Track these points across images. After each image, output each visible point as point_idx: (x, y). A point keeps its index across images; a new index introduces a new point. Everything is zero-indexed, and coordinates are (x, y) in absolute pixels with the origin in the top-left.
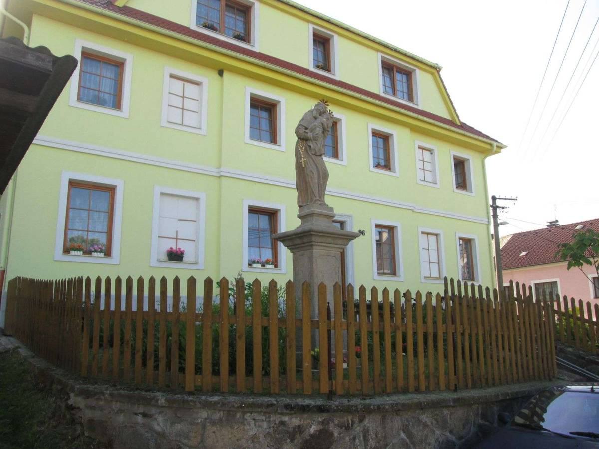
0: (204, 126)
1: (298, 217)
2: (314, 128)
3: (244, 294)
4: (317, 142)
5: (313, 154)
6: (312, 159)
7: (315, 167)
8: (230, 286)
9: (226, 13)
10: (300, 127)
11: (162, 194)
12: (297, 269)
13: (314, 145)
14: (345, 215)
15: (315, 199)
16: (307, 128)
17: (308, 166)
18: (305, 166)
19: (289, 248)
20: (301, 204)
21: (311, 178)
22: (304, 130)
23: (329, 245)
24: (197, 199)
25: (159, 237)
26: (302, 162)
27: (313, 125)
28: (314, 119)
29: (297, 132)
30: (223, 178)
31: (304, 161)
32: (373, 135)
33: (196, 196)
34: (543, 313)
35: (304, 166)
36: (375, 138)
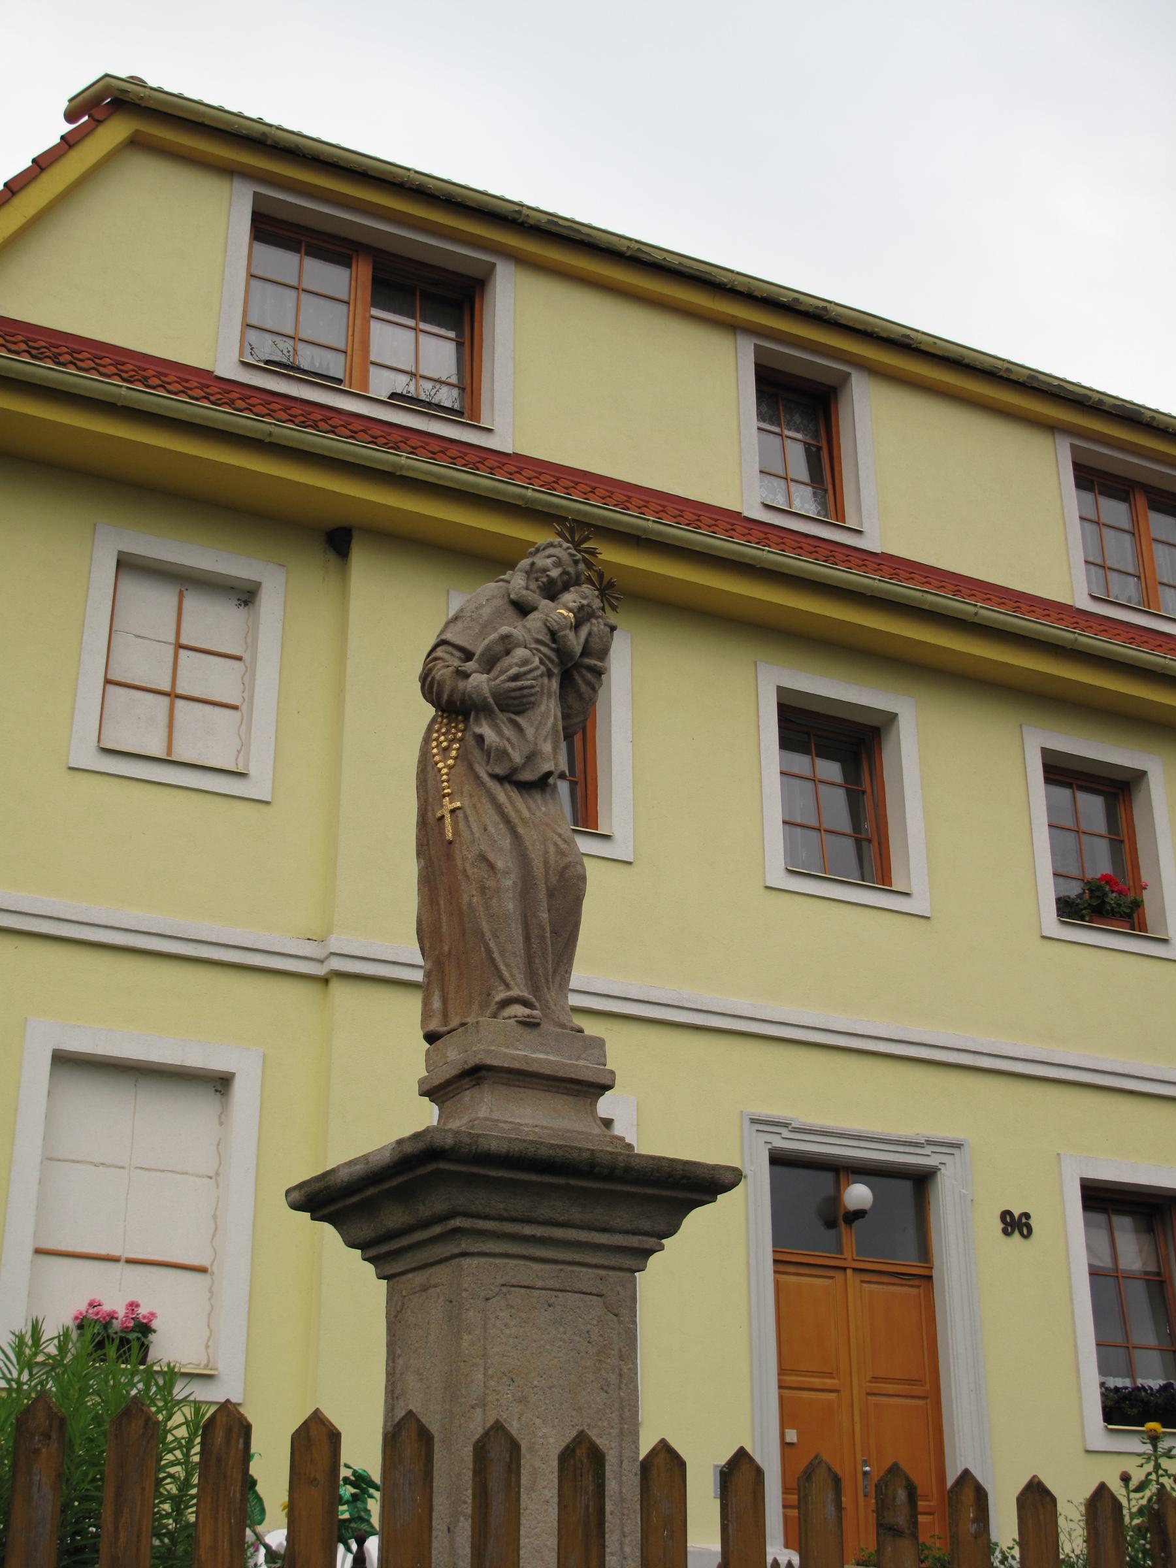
0: (260, 766)
1: (421, 1095)
2: (499, 648)
3: (76, 1501)
4: (519, 719)
5: (495, 777)
6: (493, 800)
7: (506, 842)
8: (377, 1494)
9: (375, 312)
10: (439, 652)
11: (64, 1061)
12: (400, 1361)
13: (499, 733)
14: (930, 1142)
15: (501, 996)
16: (468, 655)
17: (466, 834)
18: (456, 832)
19: (372, 1252)
20: (435, 1025)
21: (483, 890)
22: (457, 663)
23: (559, 1233)
24: (221, 1083)
25: (38, 1251)
26: (443, 817)
27: (494, 636)
28: (511, 612)
29: (430, 688)
30: (338, 989)
31: (453, 811)
32: (1048, 780)
33: (218, 1063)
34: (971, 1515)
35: (449, 835)
36: (1064, 793)
